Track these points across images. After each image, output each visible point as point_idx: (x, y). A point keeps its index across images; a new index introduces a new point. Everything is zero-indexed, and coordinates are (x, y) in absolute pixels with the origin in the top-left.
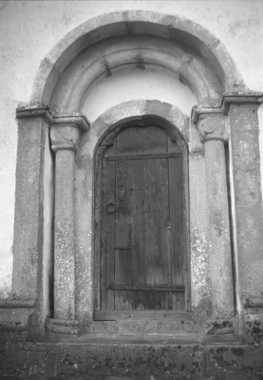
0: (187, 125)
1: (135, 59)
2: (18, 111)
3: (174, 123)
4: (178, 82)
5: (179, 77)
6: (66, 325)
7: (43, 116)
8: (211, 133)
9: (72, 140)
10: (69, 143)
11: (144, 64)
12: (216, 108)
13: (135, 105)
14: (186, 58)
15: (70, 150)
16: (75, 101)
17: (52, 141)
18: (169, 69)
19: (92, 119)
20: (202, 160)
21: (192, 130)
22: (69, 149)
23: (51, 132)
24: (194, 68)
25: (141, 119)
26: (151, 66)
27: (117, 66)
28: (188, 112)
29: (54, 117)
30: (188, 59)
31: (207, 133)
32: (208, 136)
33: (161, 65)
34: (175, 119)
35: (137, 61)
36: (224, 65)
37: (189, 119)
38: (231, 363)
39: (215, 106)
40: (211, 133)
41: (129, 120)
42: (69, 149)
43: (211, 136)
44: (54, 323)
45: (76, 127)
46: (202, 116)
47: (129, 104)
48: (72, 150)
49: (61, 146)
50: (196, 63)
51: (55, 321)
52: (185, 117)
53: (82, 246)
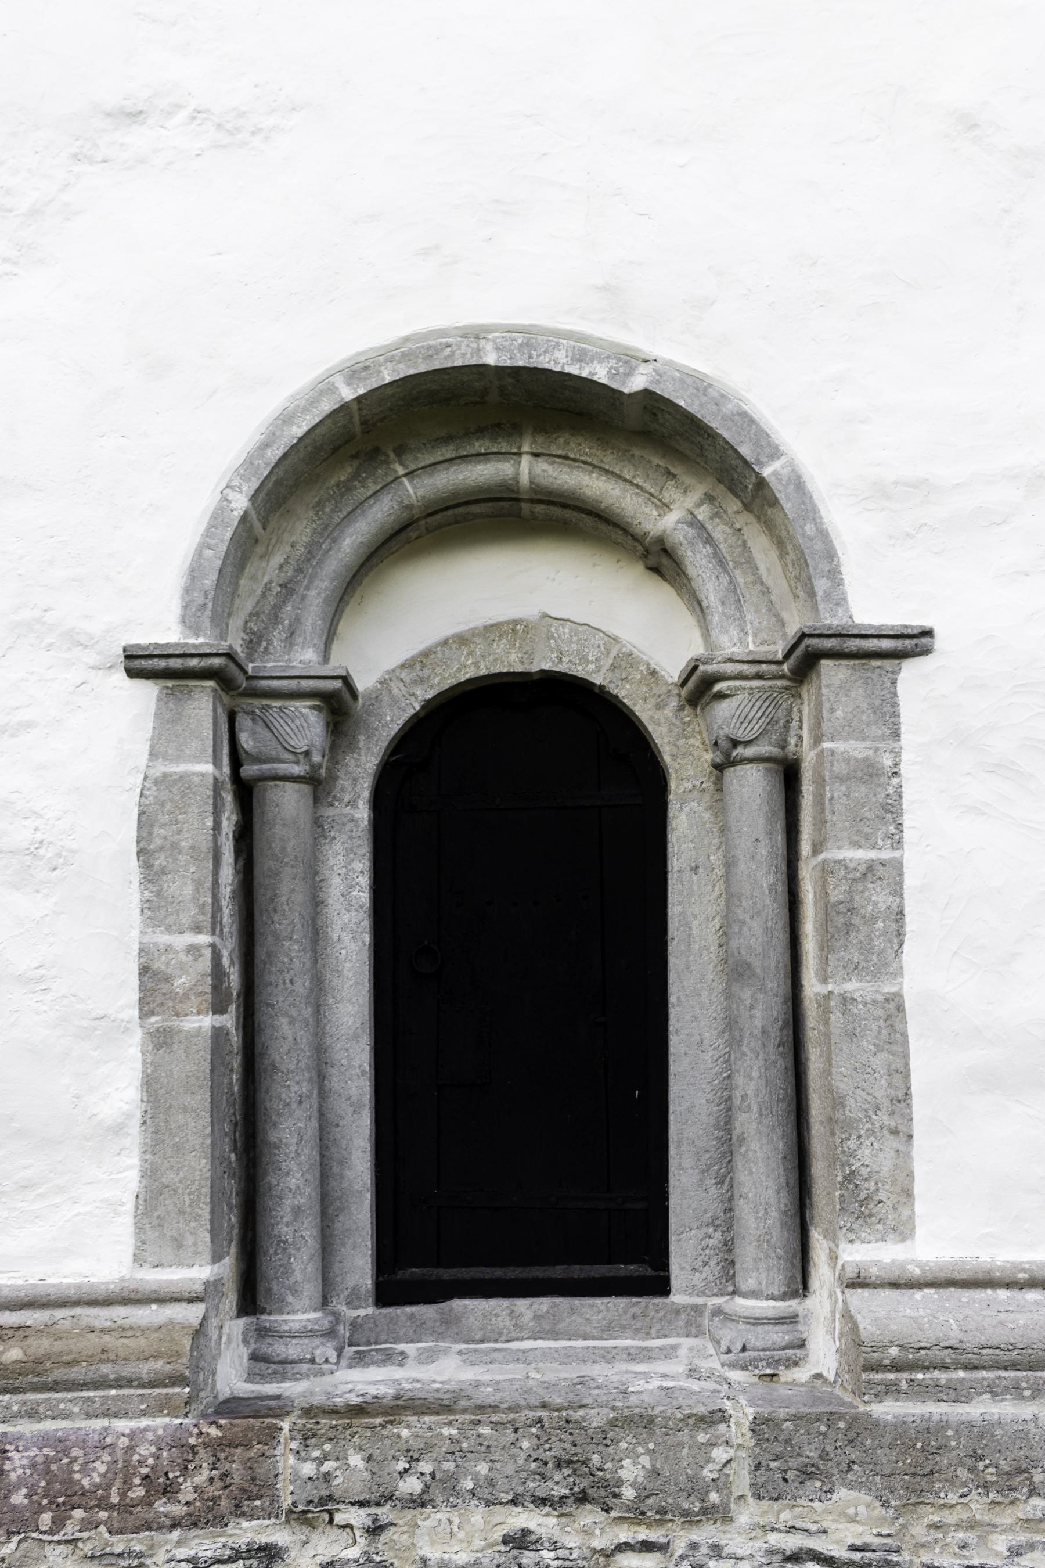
8: (747, 743)
9: (307, 754)
10: (297, 763)
27: (447, 508)
29: (249, 678)
31: (735, 743)
32: (740, 751)
43: (749, 752)
46: (718, 687)
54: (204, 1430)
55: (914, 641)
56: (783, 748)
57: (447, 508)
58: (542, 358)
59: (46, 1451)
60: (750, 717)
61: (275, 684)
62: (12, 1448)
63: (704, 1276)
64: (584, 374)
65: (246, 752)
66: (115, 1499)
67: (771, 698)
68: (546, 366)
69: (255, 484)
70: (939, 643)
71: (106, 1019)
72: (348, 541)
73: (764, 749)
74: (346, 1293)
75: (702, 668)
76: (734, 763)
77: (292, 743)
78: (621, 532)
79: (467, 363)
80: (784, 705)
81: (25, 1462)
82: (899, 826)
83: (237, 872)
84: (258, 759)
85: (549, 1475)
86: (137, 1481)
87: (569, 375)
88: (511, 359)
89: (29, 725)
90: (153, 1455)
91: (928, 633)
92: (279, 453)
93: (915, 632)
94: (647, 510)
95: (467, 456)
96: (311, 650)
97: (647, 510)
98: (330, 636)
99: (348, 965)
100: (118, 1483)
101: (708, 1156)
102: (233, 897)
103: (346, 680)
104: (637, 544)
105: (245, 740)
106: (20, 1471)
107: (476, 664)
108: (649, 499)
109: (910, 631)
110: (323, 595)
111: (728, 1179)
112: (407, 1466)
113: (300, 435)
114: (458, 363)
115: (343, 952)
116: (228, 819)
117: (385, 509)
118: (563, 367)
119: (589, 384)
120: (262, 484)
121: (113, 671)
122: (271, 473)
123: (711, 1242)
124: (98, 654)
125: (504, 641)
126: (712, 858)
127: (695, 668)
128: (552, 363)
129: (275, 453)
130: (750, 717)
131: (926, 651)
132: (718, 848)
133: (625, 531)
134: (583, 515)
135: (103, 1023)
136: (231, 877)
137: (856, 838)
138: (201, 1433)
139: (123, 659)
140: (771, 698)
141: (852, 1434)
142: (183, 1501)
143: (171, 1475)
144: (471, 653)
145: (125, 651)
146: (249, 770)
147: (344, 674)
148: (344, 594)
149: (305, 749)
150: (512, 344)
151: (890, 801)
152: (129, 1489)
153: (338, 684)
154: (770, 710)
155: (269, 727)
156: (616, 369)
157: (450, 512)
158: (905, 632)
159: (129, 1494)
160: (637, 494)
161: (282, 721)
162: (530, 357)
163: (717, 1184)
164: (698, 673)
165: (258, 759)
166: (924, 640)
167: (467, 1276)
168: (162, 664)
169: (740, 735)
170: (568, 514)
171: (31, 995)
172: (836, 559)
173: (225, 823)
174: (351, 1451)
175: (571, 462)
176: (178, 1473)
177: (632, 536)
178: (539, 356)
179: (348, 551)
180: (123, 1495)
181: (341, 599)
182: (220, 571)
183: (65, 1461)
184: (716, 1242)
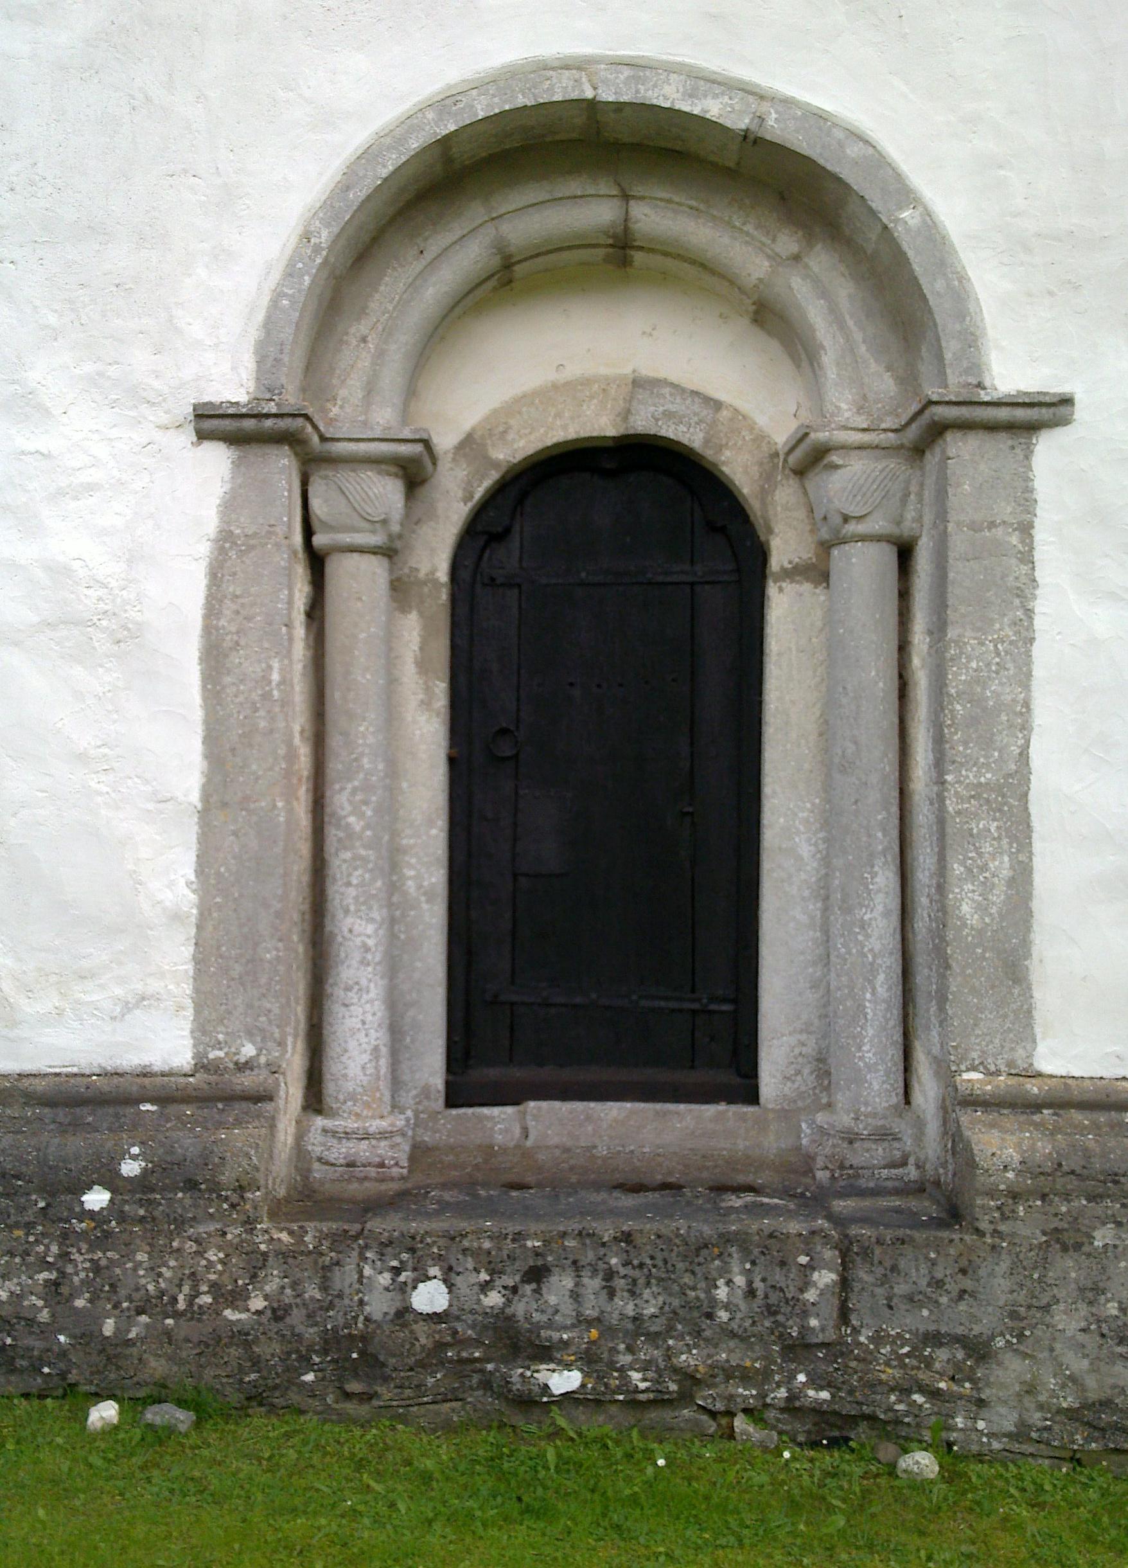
0: (768, 479)
1: (606, 234)
2: (196, 407)
3: (725, 469)
4: (745, 322)
5: (752, 308)
6: (367, 1136)
7: (289, 439)
8: (860, 518)
9: (385, 522)
10: (373, 532)
11: (632, 253)
12: (885, 430)
13: (592, 397)
14: (787, 243)
15: (374, 553)
16: (392, 376)
17: (315, 524)
18: (714, 273)
19: (445, 441)
20: (820, 594)
21: (786, 494)
22: (374, 551)
23: (311, 490)
24: (816, 281)
25: (611, 444)
26: (657, 260)
27: (538, 255)
28: (781, 437)
29: (323, 439)
30: (794, 248)
31: (846, 519)
32: (852, 528)
33: (693, 262)
34: (728, 453)
35: (610, 241)
36: (933, 287)
37: (777, 454)
38: (876, 1262)
39: (883, 426)
40: (860, 518)
41: (571, 448)
42: (374, 551)
43: (861, 528)
44: (325, 1131)
45: (396, 475)
46: (835, 458)
47: (574, 389)
48: (384, 555)
49: (347, 538)
50: (821, 260)
51: (329, 1123)
52: (765, 448)
53: (411, 866)
54: (275, 1237)
55: (1052, 410)
56: (898, 524)
57: (538, 255)
58: (650, 92)
59: (109, 1254)
60: (864, 489)
61: (352, 447)
62: (75, 1250)
63: (796, 1086)
64: (696, 111)
65: (320, 521)
66: (181, 1305)
67: (888, 470)
68: (655, 102)
69: (336, 230)
70: (1080, 412)
71: (172, 802)
72: (431, 291)
73: (877, 524)
74: (414, 1092)
75: (812, 435)
76: (844, 542)
77: (370, 511)
78: (727, 284)
79: (568, 98)
80: (901, 478)
81: (87, 1265)
82: (1029, 613)
83: (307, 646)
84: (329, 528)
85: (638, 1292)
86: (204, 1288)
87: (679, 112)
88: (615, 93)
89: (91, 488)
90: (221, 1261)
91: (1066, 401)
92: (363, 195)
93: (1054, 400)
94: (757, 261)
95: (561, 199)
96: (389, 410)
97: (757, 261)
98: (411, 392)
99: (423, 747)
100: (186, 1289)
101: (802, 958)
102: (303, 675)
103: (426, 443)
104: (744, 297)
105: (317, 505)
106: (83, 1275)
107: (565, 427)
108: (760, 249)
109: (1047, 399)
110: (403, 350)
111: (824, 983)
112: (488, 1278)
113: (384, 176)
114: (558, 98)
115: (418, 732)
116: (300, 591)
117: (472, 256)
118: (673, 103)
119: (701, 121)
120: (343, 229)
121: (181, 430)
122: (352, 217)
123: (804, 1050)
124: (166, 413)
125: (595, 401)
126: (814, 640)
127: (807, 434)
128: (661, 98)
129: (359, 194)
130: (864, 489)
131: (1064, 421)
132: (821, 630)
133: (732, 283)
134: (686, 265)
135: (169, 805)
136: (301, 653)
137: (979, 624)
138: (272, 1239)
139: (192, 418)
140: (888, 470)
141: (964, 1262)
142: (253, 1310)
143: (240, 1282)
144: (558, 415)
145: (194, 410)
146: (318, 540)
147: (425, 436)
148: (424, 348)
149: (383, 517)
150: (617, 78)
151: (1018, 585)
152: (197, 1296)
153: (419, 448)
154: (886, 482)
155: (343, 493)
156: (731, 106)
157: (540, 260)
158: (1042, 399)
159: (197, 1300)
160: (747, 242)
161: (358, 487)
162: (637, 92)
163: (811, 988)
164: (808, 441)
165: (329, 528)
166: (1063, 410)
167: (612, 1111)
168: (227, 424)
169: (852, 510)
170: (669, 263)
171: (93, 776)
172: (968, 319)
173: (297, 595)
174: (430, 1262)
175: (676, 207)
176: (247, 1281)
177: (739, 288)
178: (647, 90)
179: (431, 302)
180: (190, 1302)
181: (421, 354)
182: (297, 324)
183: (129, 1265)
184: (810, 1050)
